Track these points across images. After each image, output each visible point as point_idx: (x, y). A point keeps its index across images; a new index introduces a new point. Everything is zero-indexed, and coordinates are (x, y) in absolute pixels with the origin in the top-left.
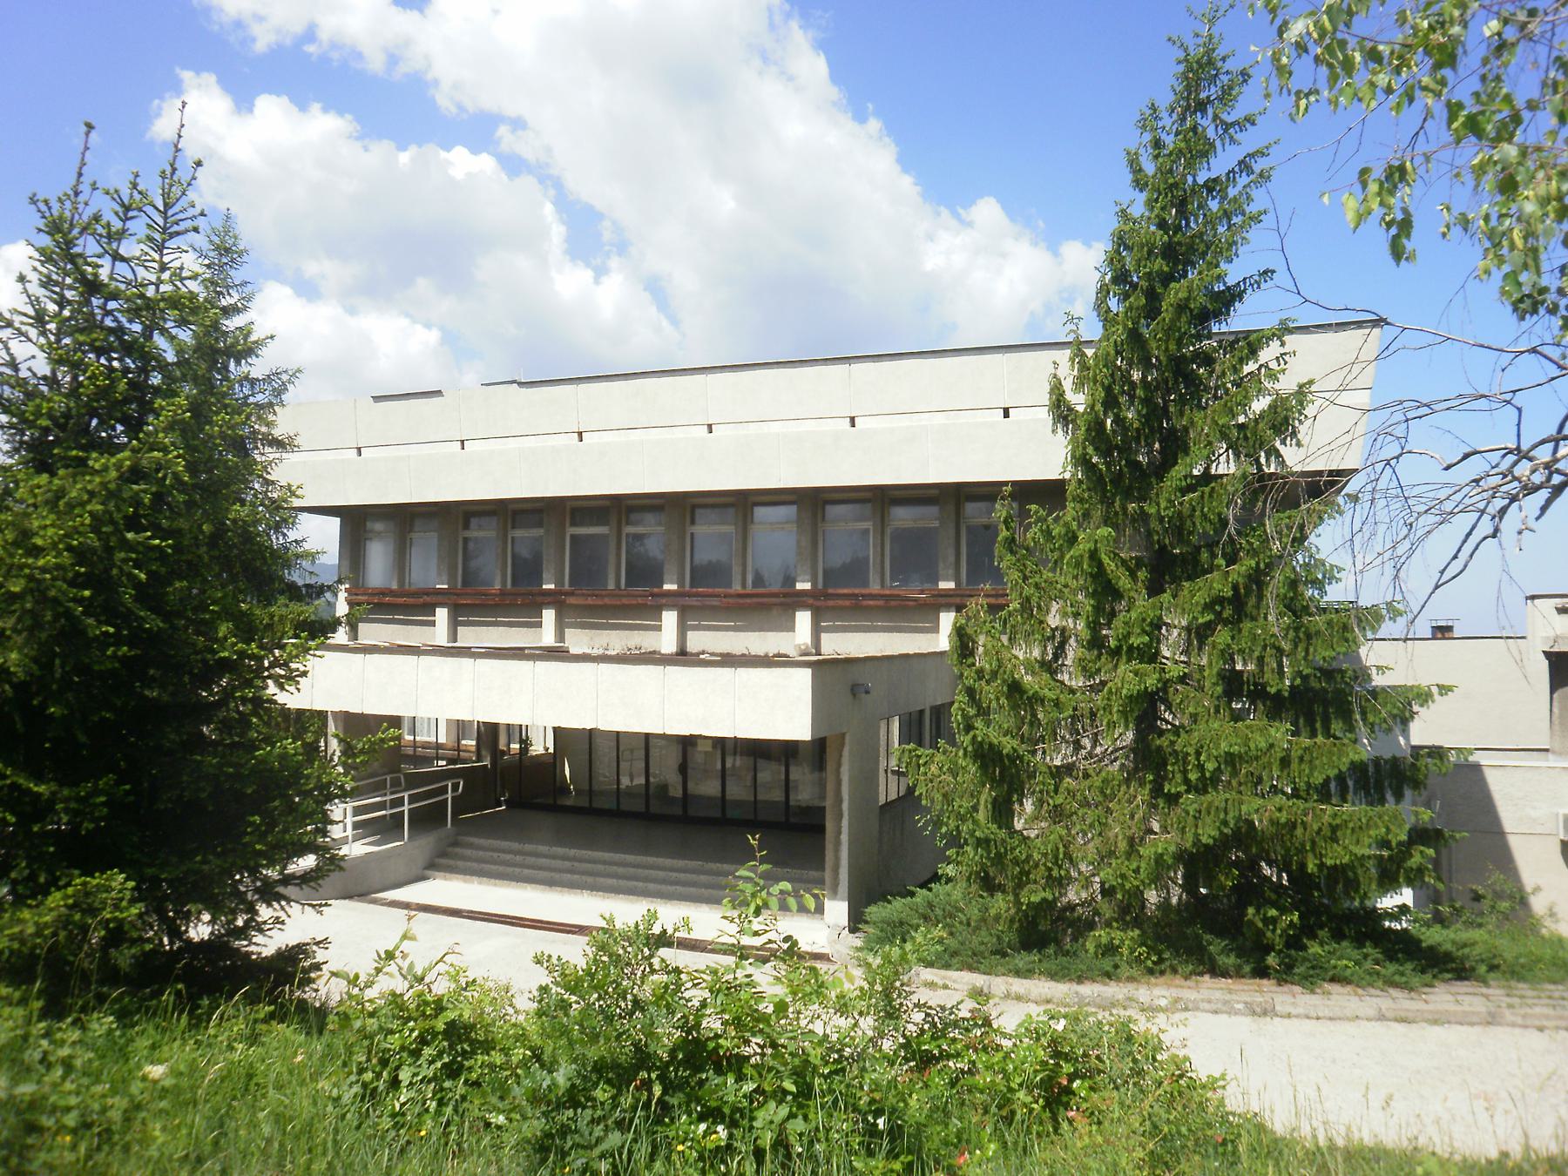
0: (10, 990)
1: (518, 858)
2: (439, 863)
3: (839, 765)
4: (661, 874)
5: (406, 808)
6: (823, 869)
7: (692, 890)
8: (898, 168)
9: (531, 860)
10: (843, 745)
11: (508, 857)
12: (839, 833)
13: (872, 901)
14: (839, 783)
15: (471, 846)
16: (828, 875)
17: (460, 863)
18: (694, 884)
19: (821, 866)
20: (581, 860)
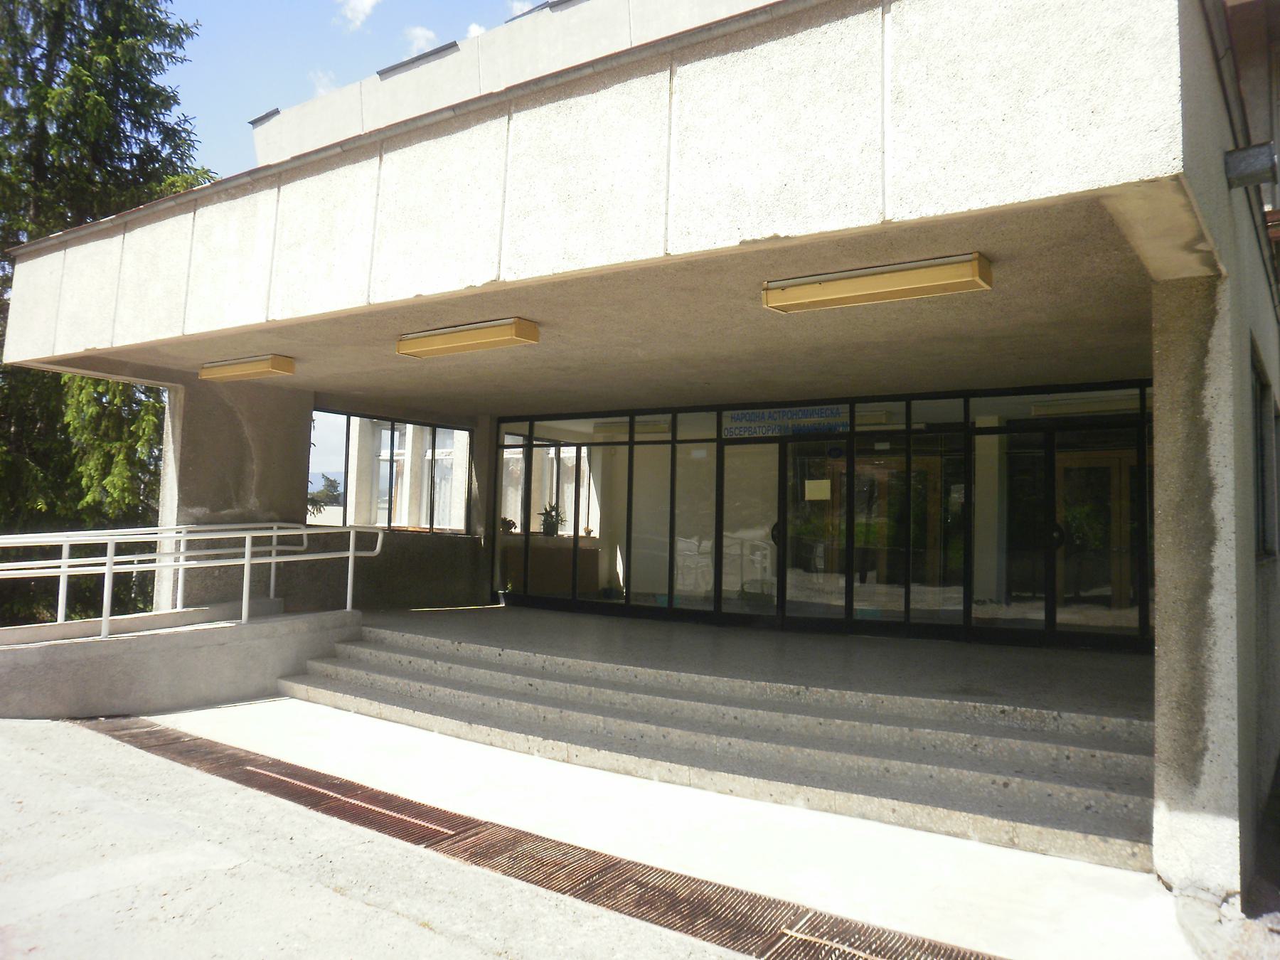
0: (1125, 797)
1: (441, 667)
2: (301, 672)
3: (1198, 378)
4: (704, 709)
5: (246, 562)
6: (1150, 717)
7: (768, 748)
8: (1243, 916)
9: (461, 671)
10: (1209, 319)
11: (426, 663)
12: (1204, 587)
13: (190, 397)
14: (1199, 434)
15: (379, 644)
16: (1165, 723)
17: (343, 671)
18: (773, 735)
19: (1139, 698)
20: (544, 674)
